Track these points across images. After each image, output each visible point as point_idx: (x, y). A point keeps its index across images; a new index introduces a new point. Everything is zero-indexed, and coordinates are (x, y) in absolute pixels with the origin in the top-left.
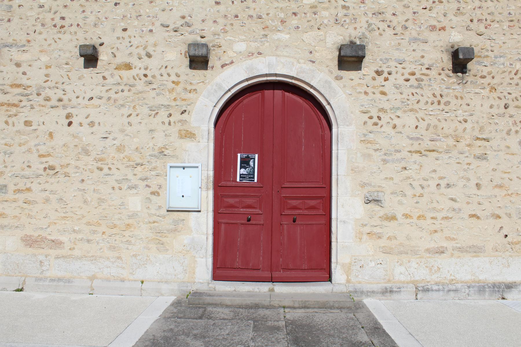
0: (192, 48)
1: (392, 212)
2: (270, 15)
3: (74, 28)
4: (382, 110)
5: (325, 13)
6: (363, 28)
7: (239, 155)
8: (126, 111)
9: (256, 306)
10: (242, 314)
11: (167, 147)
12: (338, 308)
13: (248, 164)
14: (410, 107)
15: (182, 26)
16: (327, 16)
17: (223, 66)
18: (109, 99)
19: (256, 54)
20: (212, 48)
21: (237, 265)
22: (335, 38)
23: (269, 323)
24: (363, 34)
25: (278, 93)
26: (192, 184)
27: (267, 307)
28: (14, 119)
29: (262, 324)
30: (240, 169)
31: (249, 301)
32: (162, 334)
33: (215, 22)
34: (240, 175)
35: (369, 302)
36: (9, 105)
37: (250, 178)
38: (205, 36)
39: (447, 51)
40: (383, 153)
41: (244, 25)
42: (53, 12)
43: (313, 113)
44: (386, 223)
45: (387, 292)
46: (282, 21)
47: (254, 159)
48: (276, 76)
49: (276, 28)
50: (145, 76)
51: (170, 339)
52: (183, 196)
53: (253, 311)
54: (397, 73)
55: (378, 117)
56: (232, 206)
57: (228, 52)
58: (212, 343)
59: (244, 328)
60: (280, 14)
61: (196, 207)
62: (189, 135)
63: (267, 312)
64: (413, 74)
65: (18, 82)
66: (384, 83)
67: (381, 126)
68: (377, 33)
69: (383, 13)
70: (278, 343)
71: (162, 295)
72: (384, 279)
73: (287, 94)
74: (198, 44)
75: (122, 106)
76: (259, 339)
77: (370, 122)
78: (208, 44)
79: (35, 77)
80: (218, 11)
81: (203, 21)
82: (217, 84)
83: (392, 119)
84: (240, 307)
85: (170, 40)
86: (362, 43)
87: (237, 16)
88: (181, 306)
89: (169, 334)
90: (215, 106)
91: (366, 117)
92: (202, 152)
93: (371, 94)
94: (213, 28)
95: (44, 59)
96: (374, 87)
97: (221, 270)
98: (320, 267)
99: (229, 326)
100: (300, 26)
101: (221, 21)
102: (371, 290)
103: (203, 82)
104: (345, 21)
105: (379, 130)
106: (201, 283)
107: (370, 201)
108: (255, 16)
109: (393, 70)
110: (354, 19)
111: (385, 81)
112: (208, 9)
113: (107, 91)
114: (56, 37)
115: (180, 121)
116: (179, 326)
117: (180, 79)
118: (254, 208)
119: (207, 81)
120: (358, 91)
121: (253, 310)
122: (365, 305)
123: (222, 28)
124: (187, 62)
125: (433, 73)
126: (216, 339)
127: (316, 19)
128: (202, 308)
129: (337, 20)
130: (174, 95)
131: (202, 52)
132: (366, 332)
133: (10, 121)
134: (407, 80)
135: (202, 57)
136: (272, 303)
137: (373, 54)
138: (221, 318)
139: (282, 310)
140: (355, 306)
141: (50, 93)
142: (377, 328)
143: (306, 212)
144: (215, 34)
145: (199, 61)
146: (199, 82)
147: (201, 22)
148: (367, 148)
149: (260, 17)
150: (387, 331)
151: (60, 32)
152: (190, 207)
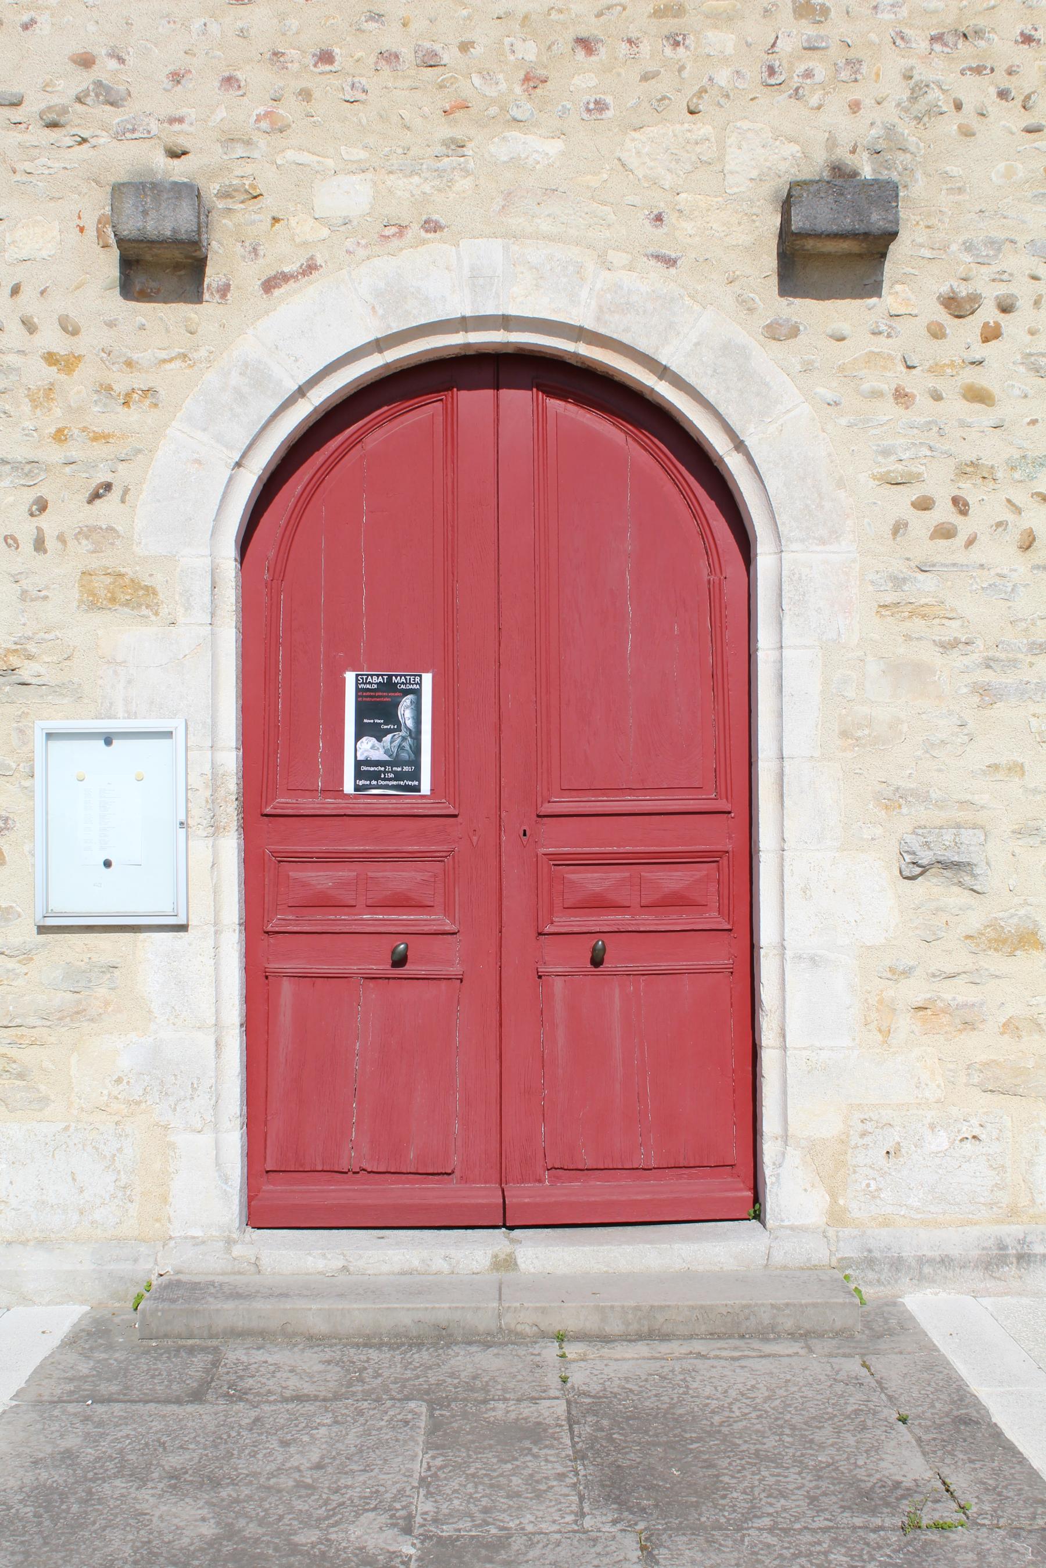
0: (128, 205)
1: (1022, 912)
2: (476, 51)
5: (721, 40)
6: (890, 106)
7: (350, 677)
9: (440, 1337)
10: (377, 1375)
11: (32, 648)
12: (793, 1336)
13: (390, 714)
15: (79, 100)
16: (730, 50)
17: (269, 286)
19: (415, 231)
20: (220, 205)
21: (349, 1158)
22: (766, 150)
23: (498, 1411)
24: (890, 131)
25: (518, 401)
26: (143, 804)
27: (486, 1341)
29: (465, 1415)
30: (358, 737)
31: (405, 1315)
32: (29, 1478)
33: (229, 81)
34: (358, 764)
35: (925, 1304)
37: (398, 776)
38: (187, 145)
40: (976, 657)
41: (362, 96)
43: (669, 487)
44: (994, 962)
45: (1005, 1259)
46: (527, 79)
47: (417, 693)
48: (507, 329)
49: (504, 109)
51: (63, 1497)
52: (107, 864)
53: (425, 1356)
54: (1037, 303)
55: (955, 501)
56: (324, 902)
57: (293, 222)
58: (250, 1507)
59: (387, 1435)
60: (519, 45)
61: (169, 910)
62: (126, 593)
63: (489, 1361)
66: (980, 351)
67: (970, 542)
68: (950, 125)
69: (978, 33)
70: (539, 1495)
71: (25, 1300)
72: (991, 1205)
73: (555, 405)
74: (154, 186)
76: (455, 1484)
77: (922, 524)
78: (201, 182)
80: (242, 34)
81: (177, 78)
82: (246, 365)
83: (1018, 510)
84: (369, 1341)
85: (28, 166)
86: (885, 175)
87: (326, 57)
88: (110, 1347)
89: (58, 1477)
90: (238, 465)
92: (186, 668)
93: (922, 401)
94: (221, 113)
96: (936, 369)
97: (284, 1185)
98: (720, 1167)
99: (323, 1431)
100: (609, 100)
101: (258, 78)
102: (935, 1254)
103: (184, 356)
104: (808, 74)
105: (961, 557)
106: (197, 1242)
107: (925, 870)
108: (407, 53)
109: (1023, 291)
110: (848, 62)
111: (986, 340)
112: (197, 25)
115: (86, 532)
116: (102, 1435)
117: (82, 345)
118: (421, 906)
119: (203, 353)
120: (866, 387)
121: (425, 1354)
122: (912, 1318)
123: (261, 110)
124: (108, 265)
126: (269, 1488)
127: (682, 69)
128: (204, 1349)
129: (771, 71)
130: (55, 416)
131: (170, 221)
132: (919, 1440)
135: (176, 242)
136: (508, 1320)
137: (933, 221)
138: (288, 1393)
139: (551, 1351)
140: (868, 1325)
142: (967, 1421)
143: (647, 921)
144: (230, 141)
145: (162, 264)
146: (164, 355)
147: (168, 85)
148: (908, 638)
149: (430, 61)
150: (1012, 1434)
152: (141, 909)
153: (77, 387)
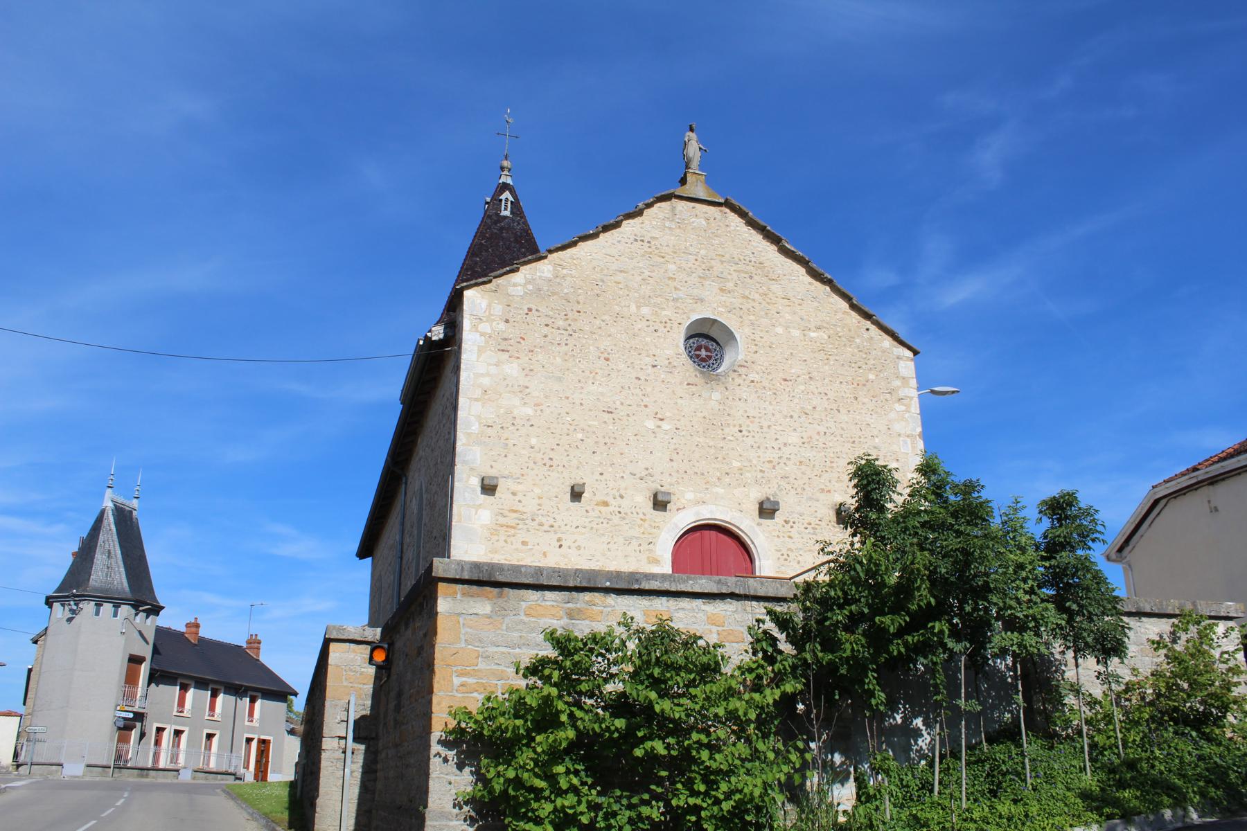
3: (560, 469)
4: (790, 549)
5: (748, 475)
8: (606, 539)
25: (713, 533)
79: (530, 505)
95: (537, 491)
114: (546, 474)
125: (823, 524)
141: (543, 520)
145: (660, 504)
153: (646, 525)
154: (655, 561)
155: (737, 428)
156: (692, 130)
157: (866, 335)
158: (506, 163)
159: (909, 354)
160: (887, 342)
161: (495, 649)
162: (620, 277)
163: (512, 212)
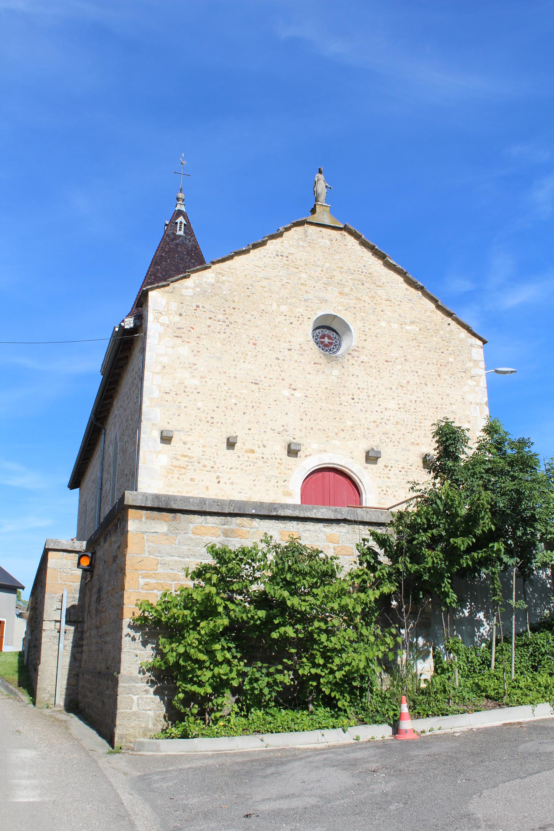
3: (219, 425)
4: (388, 487)
5: (358, 431)
14: (402, 486)
17: (306, 457)
18: (242, 469)
22: (364, 446)
25: (332, 474)
28: (183, 476)
36: (180, 467)
39: (420, 457)
42: (206, 413)
50: (263, 458)
64: (403, 468)
65: (185, 454)
68: (385, 444)
75: (250, 474)
77: (382, 493)
81: (294, 429)
87: (312, 429)
91: (380, 490)
93: (382, 478)
96: (384, 474)
101: (303, 430)
109: (393, 465)
113: (241, 465)
114: (209, 428)
115: (283, 486)
117: (282, 462)
125: (413, 468)
133: (181, 477)
134: (400, 471)
141: (206, 463)
145: (292, 452)
149: (324, 430)
151: (211, 426)
153: (282, 467)
154: (289, 494)
155: (351, 396)
156: (320, 172)
157: (448, 328)
158: (181, 195)
159: (480, 343)
160: (464, 333)
161: (170, 558)
162: (265, 283)
163: (185, 232)
